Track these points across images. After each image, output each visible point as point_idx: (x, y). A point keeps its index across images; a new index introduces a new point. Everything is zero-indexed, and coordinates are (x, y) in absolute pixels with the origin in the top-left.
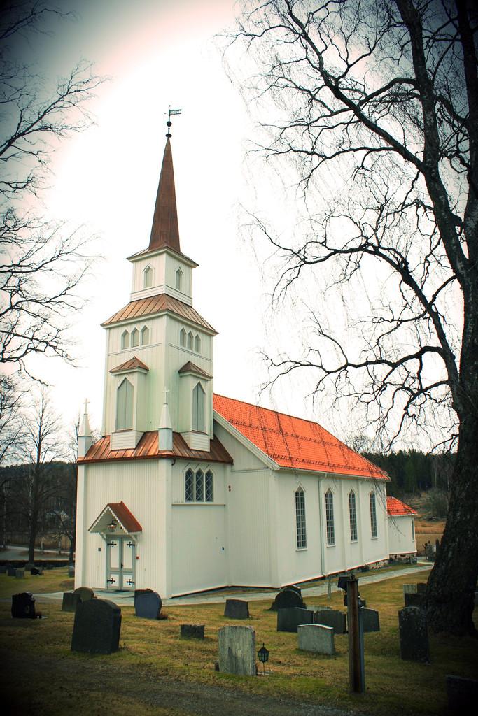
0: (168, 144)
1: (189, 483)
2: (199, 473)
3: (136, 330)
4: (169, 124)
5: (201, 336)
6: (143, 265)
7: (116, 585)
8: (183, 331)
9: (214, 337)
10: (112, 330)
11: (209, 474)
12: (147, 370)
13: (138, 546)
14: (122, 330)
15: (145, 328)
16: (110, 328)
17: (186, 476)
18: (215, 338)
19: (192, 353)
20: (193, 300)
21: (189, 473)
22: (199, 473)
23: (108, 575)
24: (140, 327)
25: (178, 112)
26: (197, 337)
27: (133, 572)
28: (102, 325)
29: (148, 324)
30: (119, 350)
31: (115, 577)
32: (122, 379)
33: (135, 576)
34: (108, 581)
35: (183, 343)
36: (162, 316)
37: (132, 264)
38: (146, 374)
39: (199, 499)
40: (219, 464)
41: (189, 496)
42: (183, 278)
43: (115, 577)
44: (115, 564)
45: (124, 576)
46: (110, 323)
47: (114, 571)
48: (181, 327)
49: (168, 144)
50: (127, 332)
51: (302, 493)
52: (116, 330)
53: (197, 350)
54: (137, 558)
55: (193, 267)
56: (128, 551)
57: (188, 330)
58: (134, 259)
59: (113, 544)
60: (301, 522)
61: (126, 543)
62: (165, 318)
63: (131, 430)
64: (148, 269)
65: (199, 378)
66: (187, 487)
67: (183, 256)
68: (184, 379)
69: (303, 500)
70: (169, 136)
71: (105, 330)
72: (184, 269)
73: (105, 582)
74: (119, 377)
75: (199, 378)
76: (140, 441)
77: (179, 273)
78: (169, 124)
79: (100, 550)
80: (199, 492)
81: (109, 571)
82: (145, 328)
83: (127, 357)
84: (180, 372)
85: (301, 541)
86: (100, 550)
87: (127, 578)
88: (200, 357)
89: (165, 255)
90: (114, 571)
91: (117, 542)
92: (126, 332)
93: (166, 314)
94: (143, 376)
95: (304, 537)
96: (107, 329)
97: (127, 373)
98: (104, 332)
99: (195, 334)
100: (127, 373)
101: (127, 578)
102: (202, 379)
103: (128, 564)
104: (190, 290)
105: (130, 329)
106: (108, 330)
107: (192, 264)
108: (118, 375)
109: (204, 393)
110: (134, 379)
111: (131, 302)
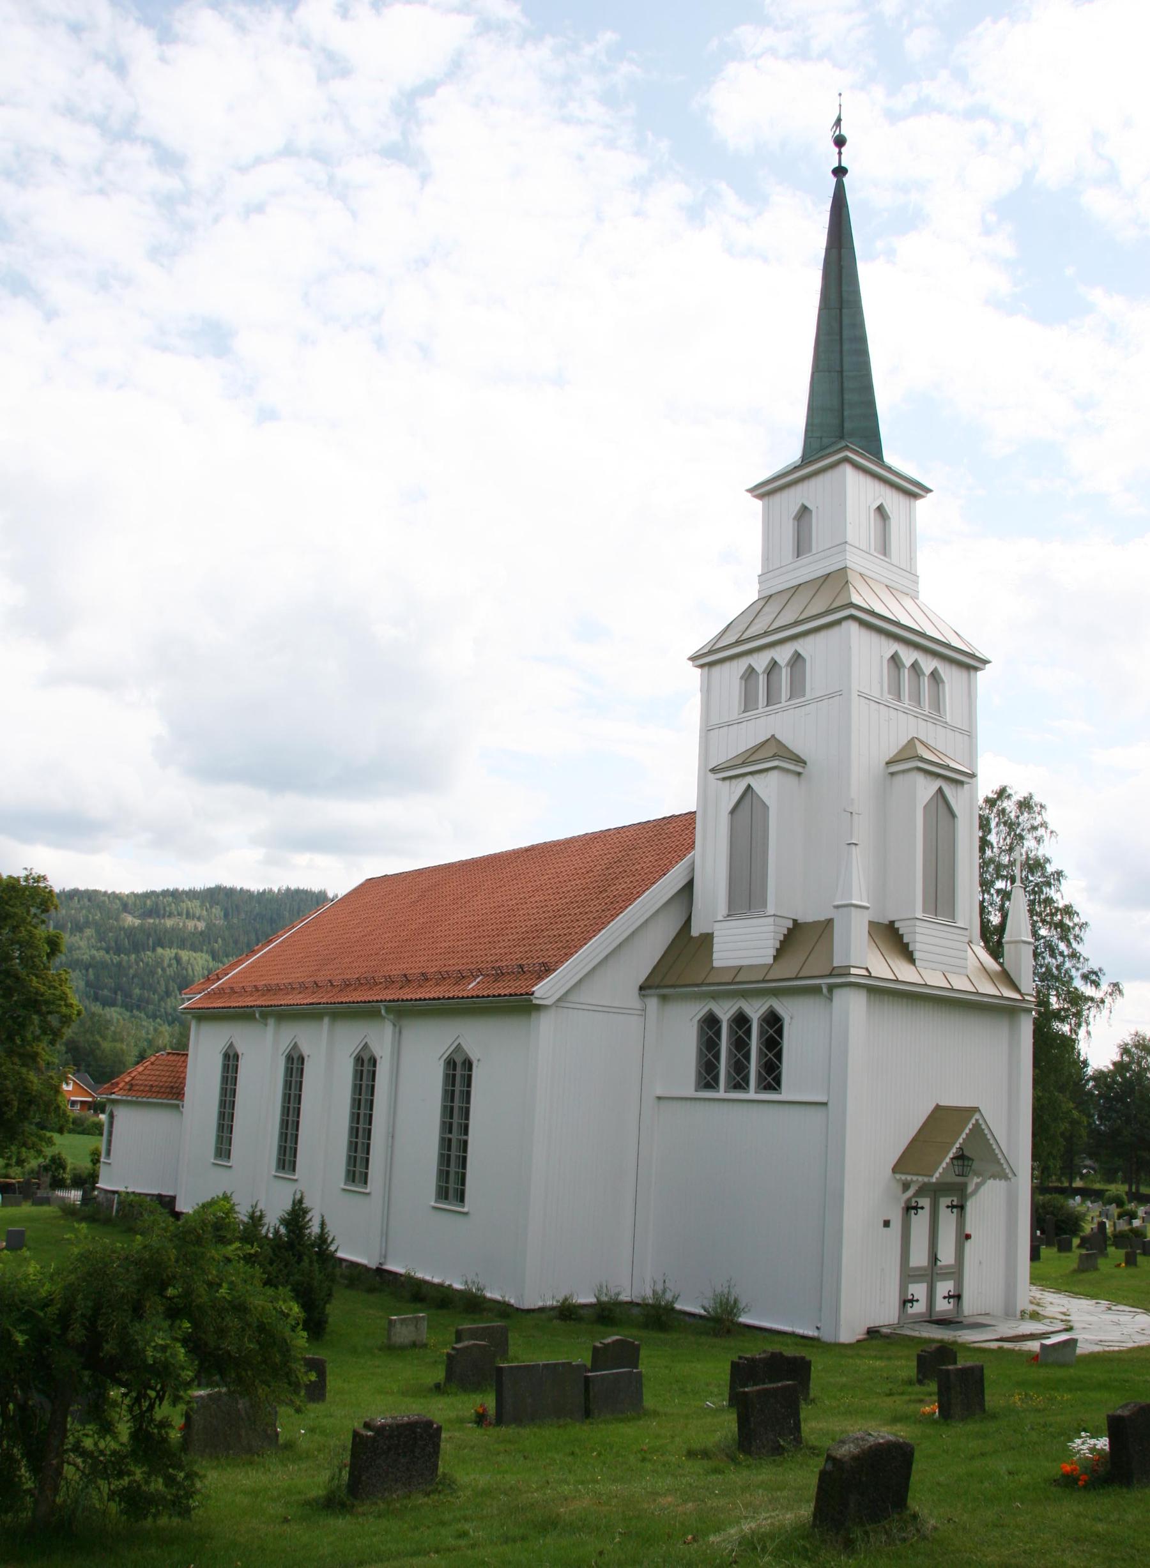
2: (741, 1020)
3: (774, 665)
5: (945, 671)
8: (895, 659)
9: (979, 673)
10: (716, 670)
11: (773, 1021)
13: (970, 1205)
14: (741, 665)
15: (797, 657)
16: (711, 664)
17: (781, 1036)
18: (982, 677)
20: (920, 579)
21: (710, 1022)
22: (741, 1020)
23: (903, 1288)
24: (783, 655)
26: (934, 675)
27: (957, 1272)
28: (692, 659)
29: (803, 646)
32: (740, 786)
33: (959, 1284)
36: (838, 622)
38: (799, 774)
41: (707, 1077)
43: (919, 1290)
44: (919, 1258)
46: (711, 652)
50: (776, 662)
52: (727, 666)
53: (937, 704)
54: (968, 1237)
56: (948, 1222)
57: (908, 656)
58: (766, 491)
60: (224, 1147)
61: (944, 1201)
66: (779, 1056)
67: (889, 469)
71: (699, 671)
72: (893, 501)
74: (734, 781)
79: (887, 1224)
80: (739, 1069)
81: (908, 1275)
82: (797, 657)
91: (925, 1202)
92: (751, 671)
94: (791, 780)
97: (751, 773)
99: (928, 665)
100: (751, 773)
101: (944, 1287)
103: (947, 1256)
104: (912, 559)
105: (760, 662)
107: (912, 490)
109: (953, 815)
110: (768, 787)
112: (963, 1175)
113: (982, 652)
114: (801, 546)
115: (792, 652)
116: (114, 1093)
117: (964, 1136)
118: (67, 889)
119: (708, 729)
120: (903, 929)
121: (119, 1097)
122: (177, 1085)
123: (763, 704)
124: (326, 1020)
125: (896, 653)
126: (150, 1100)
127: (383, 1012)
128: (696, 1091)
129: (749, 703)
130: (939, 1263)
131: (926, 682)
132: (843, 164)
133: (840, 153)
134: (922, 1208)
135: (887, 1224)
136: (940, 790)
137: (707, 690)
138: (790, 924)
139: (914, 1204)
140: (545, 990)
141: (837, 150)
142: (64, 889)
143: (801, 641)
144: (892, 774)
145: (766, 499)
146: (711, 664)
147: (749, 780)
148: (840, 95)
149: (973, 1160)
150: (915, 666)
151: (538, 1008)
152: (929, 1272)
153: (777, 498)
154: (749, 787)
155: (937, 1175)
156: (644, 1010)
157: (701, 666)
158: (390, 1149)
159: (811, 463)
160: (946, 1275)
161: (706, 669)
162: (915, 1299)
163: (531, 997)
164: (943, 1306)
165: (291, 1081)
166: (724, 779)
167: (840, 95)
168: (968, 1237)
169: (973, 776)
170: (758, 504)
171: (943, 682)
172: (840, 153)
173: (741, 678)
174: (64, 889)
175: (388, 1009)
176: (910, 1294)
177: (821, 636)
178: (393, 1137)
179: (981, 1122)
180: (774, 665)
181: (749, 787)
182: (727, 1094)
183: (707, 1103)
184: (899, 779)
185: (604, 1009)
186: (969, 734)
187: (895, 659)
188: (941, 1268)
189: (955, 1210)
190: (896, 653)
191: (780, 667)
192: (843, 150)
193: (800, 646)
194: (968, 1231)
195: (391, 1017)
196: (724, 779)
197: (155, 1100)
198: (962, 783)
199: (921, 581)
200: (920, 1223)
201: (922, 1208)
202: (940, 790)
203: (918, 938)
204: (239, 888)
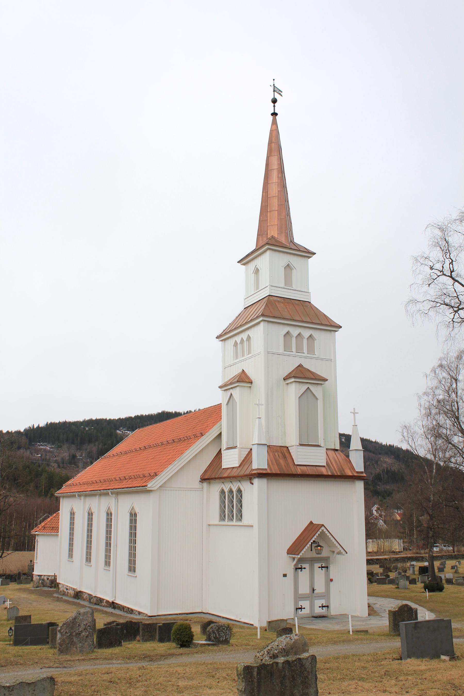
0: (274, 123)
1: (222, 502)
2: (231, 491)
4: (274, 101)
6: (252, 266)
7: (306, 611)
11: (239, 491)
13: (332, 568)
18: (339, 334)
21: (223, 492)
22: (231, 491)
23: (296, 602)
25: (271, 86)
27: (326, 595)
28: (217, 338)
30: (281, 350)
31: (305, 604)
33: (328, 599)
34: (297, 609)
35: (287, 347)
36: (259, 323)
37: (244, 267)
38: (250, 387)
40: (217, 481)
41: (222, 517)
43: (305, 604)
44: (304, 589)
45: (316, 601)
47: (304, 597)
49: (274, 123)
54: (331, 580)
55: (310, 257)
56: (320, 574)
58: (245, 261)
59: (301, 568)
61: (317, 565)
62: (262, 324)
63: (235, 447)
64: (257, 271)
70: (274, 114)
72: (295, 261)
73: (292, 609)
76: (243, 461)
78: (274, 101)
81: (298, 597)
83: (236, 371)
85: (71, 555)
86: (285, 575)
87: (319, 603)
88: (317, 359)
89: (268, 253)
90: (304, 597)
91: (306, 566)
93: (263, 320)
96: (222, 341)
98: (219, 343)
100: (232, 388)
101: (319, 603)
103: (320, 588)
106: (223, 342)
107: (308, 254)
108: (226, 390)
112: (320, 554)
116: (36, 531)
118: (87, 419)
121: (39, 533)
122: (55, 526)
123: (246, 354)
124: (97, 497)
126: (52, 533)
127: (110, 494)
128: (219, 522)
130: (315, 592)
132: (276, 112)
133: (274, 106)
134: (305, 568)
135: (285, 575)
139: (300, 567)
140: (151, 485)
141: (273, 105)
142: (85, 419)
144: (287, 384)
147: (231, 391)
148: (274, 80)
149: (323, 547)
151: (149, 491)
155: (301, 554)
156: (203, 488)
158: (115, 551)
160: (320, 596)
162: (321, 608)
163: (146, 487)
164: (318, 611)
165: (132, 519)
166: (224, 390)
167: (274, 80)
168: (331, 580)
172: (274, 106)
173: (234, 346)
174: (85, 419)
175: (112, 493)
176: (300, 605)
178: (117, 546)
179: (325, 530)
182: (228, 523)
183: (248, 527)
184: (290, 385)
185: (194, 489)
186: (331, 360)
189: (323, 569)
192: (276, 104)
193: (248, 332)
195: (114, 495)
197: (54, 533)
200: (304, 575)
201: (305, 568)
204: (174, 412)
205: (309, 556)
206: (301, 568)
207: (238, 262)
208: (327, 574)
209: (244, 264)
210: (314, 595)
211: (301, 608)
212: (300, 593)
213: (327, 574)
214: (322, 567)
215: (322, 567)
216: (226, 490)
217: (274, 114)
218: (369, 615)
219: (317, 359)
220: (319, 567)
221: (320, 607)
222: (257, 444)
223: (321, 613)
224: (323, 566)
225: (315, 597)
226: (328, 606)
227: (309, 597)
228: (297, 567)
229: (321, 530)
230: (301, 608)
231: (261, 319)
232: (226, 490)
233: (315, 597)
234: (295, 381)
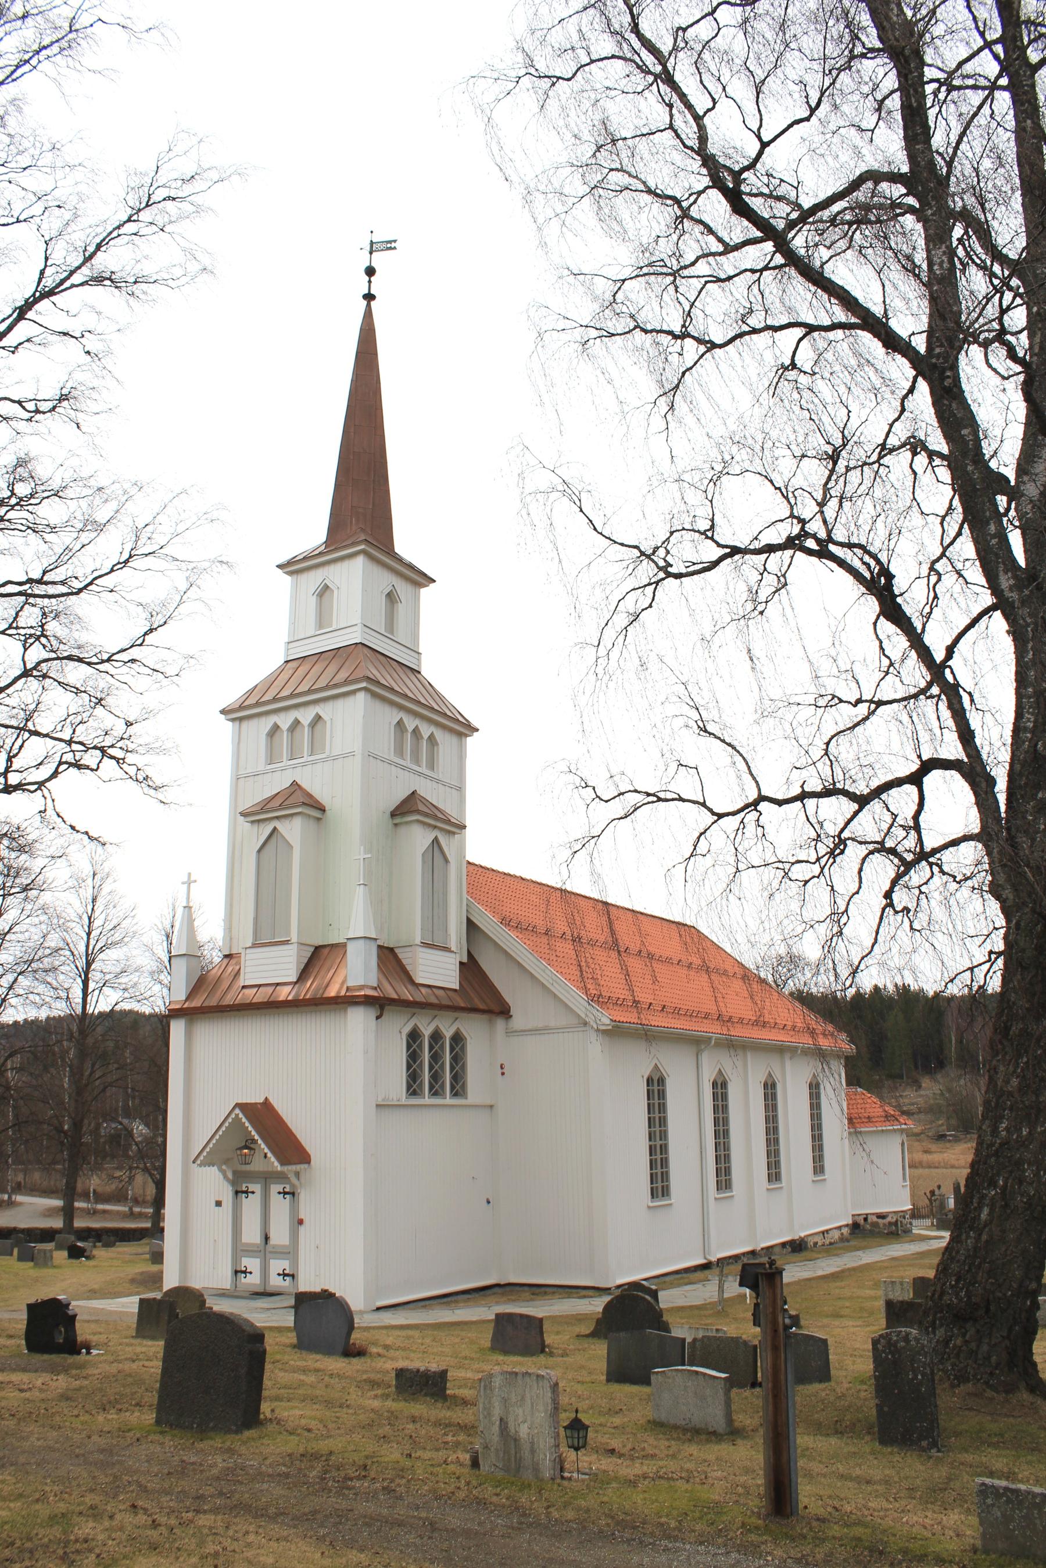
0: (368, 314)
1: (413, 1057)
2: (436, 1036)
3: (297, 723)
4: (370, 272)
5: (439, 735)
6: (313, 580)
8: (400, 724)
11: (458, 1039)
12: (323, 810)
13: (303, 1196)
14: (267, 723)
15: (318, 718)
19: (420, 774)
21: (414, 1036)
22: (436, 1036)
24: (306, 716)
27: (291, 1252)
29: (324, 710)
31: (252, 1264)
32: (268, 829)
33: (295, 1263)
35: (400, 751)
37: (288, 578)
38: (319, 819)
39: (435, 1093)
42: (401, 609)
44: (251, 1235)
46: (241, 708)
47: (250, 1251)
48: (396, 716)
49: (368, 314)
51: (661, 1081)
53: (431, 766)
54: (301, 1222)
56: (280, 1206)
57: (411, 723)
58: (293, 567)
59: (246, 1192)
61: (275, 1188)
64: (324, 591)
65: (435, 827)
68: (402, 830)
69: (662, 1094)
70: (369, 297)
71: (230, 723)
72: (403, 589)
73: (229, 1273)
74: (262, 825)
75: (435, 827)
77: (391, 597)
78: (370, 272)
79: (219, 1204)
81: (239, 1249)
82: (318, 718)
83: (278, 783)
84: (393, 815)
86: (219, 1204)
87: (278, 1265)
88: (438, 781)
90: (250, 1251)
91: (256, 1187)
92: (276, 728)
93: (365, 689)
94: (312, 823)
95: (665, 1176)
97: (277, 818)
99: (426, 730)
100: (277, 818)
101: (278, 1265)
102: (441, 829)
103: (280, 1236)
105: (285, 721)
107: (420, 579)
108: (259, 821)
109: (446, 861)
110: (293, 830)
111: (287, 662)
113: (475, 723)
114: (322, 619)
115: (314, 714)
117: (250, 1128)
119: (237, 779)
120: (402, 954)
125: (432, 734)
129: (272, 757)
131: (409, 736)
133: (370, 282)
134: (253, 1193)
136: (436, 838)
137: (238, 742)
138: (312, 949)
139: (244, 1189)
141: (367, 278)
143: (322, 705)
145: (295, 576)
146: (241, 719)
150: (416, 731)
152: (262, 1248)
153: (304, 577)
154: (275, 829)
157: (233, 720)
159: (336, 550)
161: (237, 723)
166: (253, 822)
169: (464, 827)
170: (286, 580)
171: (437, 744)
172: (370, 282)
177: (340, 703)
180: (297, 723)
181: (275, 829)
186: (460, 789)
187: (400, 724)
188: (274, 1246)
190: (432, 734)
191: (303, 726)
192: (372, 279)
194: (301, 1216)
196: (253, 822)
198: (454, 833)
199: (423, 658)
200: (251, 1206)
201: (253, 1193)
202: (436, 838)
203: (421, 968)
205: (261, 1169)
206: (246, 1192)
207: (278, 566)
208: (294, 1209)
209: (290, 573)
210: (269, 1248)
211: (245, 1272)
212: (243, 1241)
213: (294, 1209)
214: (285, 1193)
215: (285, 1193)
216: (427, 1032)
217: (369, 297)
218: (32, 1261)
219: (438, 781)
220: (279, 1193)
221: (251, 1273)
222: (365, 937)
223: (280, 1287)
224: (287, 1190)
225: (270, 1252)
226: (293, 1276)
227: (242, 1250)
228: (239, 1189)
229: (233, 1116)
230: (245, 1272)
231: (364, 685)
232: (427, 1032)
233: (270, 1252)
234: (418, 821)
